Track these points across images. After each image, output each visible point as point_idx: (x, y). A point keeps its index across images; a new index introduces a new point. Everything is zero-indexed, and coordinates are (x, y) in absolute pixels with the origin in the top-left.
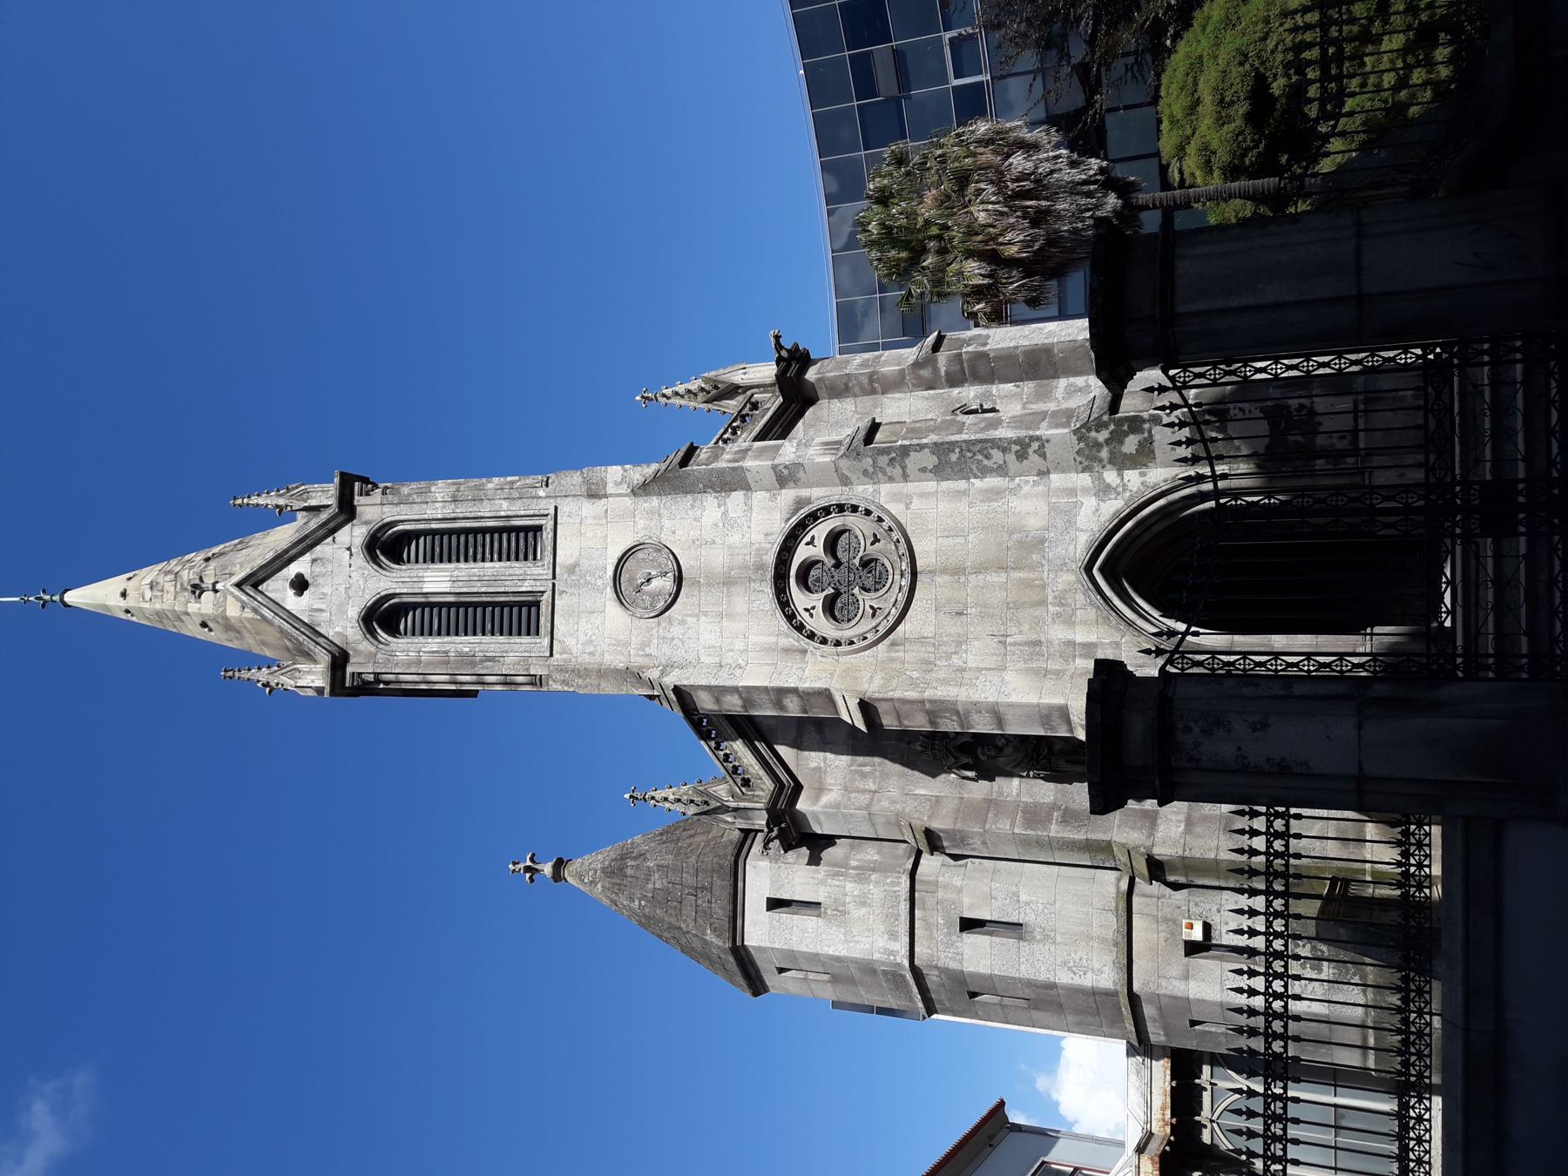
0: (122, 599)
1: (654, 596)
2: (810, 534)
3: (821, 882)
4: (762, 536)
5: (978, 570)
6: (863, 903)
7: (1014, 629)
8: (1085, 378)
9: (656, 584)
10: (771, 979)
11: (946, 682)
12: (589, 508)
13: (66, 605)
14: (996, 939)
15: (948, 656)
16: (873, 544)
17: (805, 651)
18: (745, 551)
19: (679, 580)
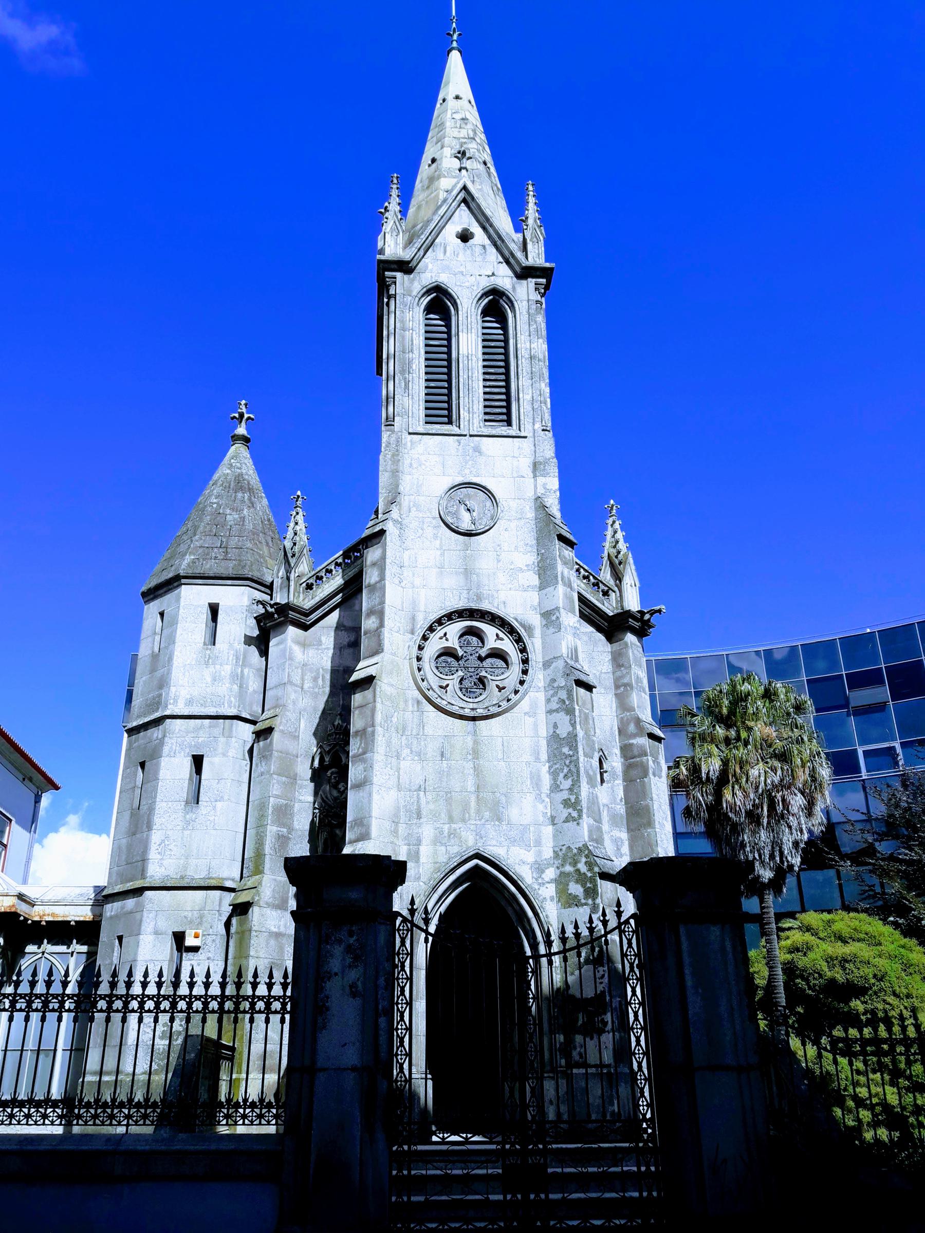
5: (477, 770)
7: (430, 797)
8: (628, 853)
11: (389, 744)
16: (497, 686)
19: (469, 534)
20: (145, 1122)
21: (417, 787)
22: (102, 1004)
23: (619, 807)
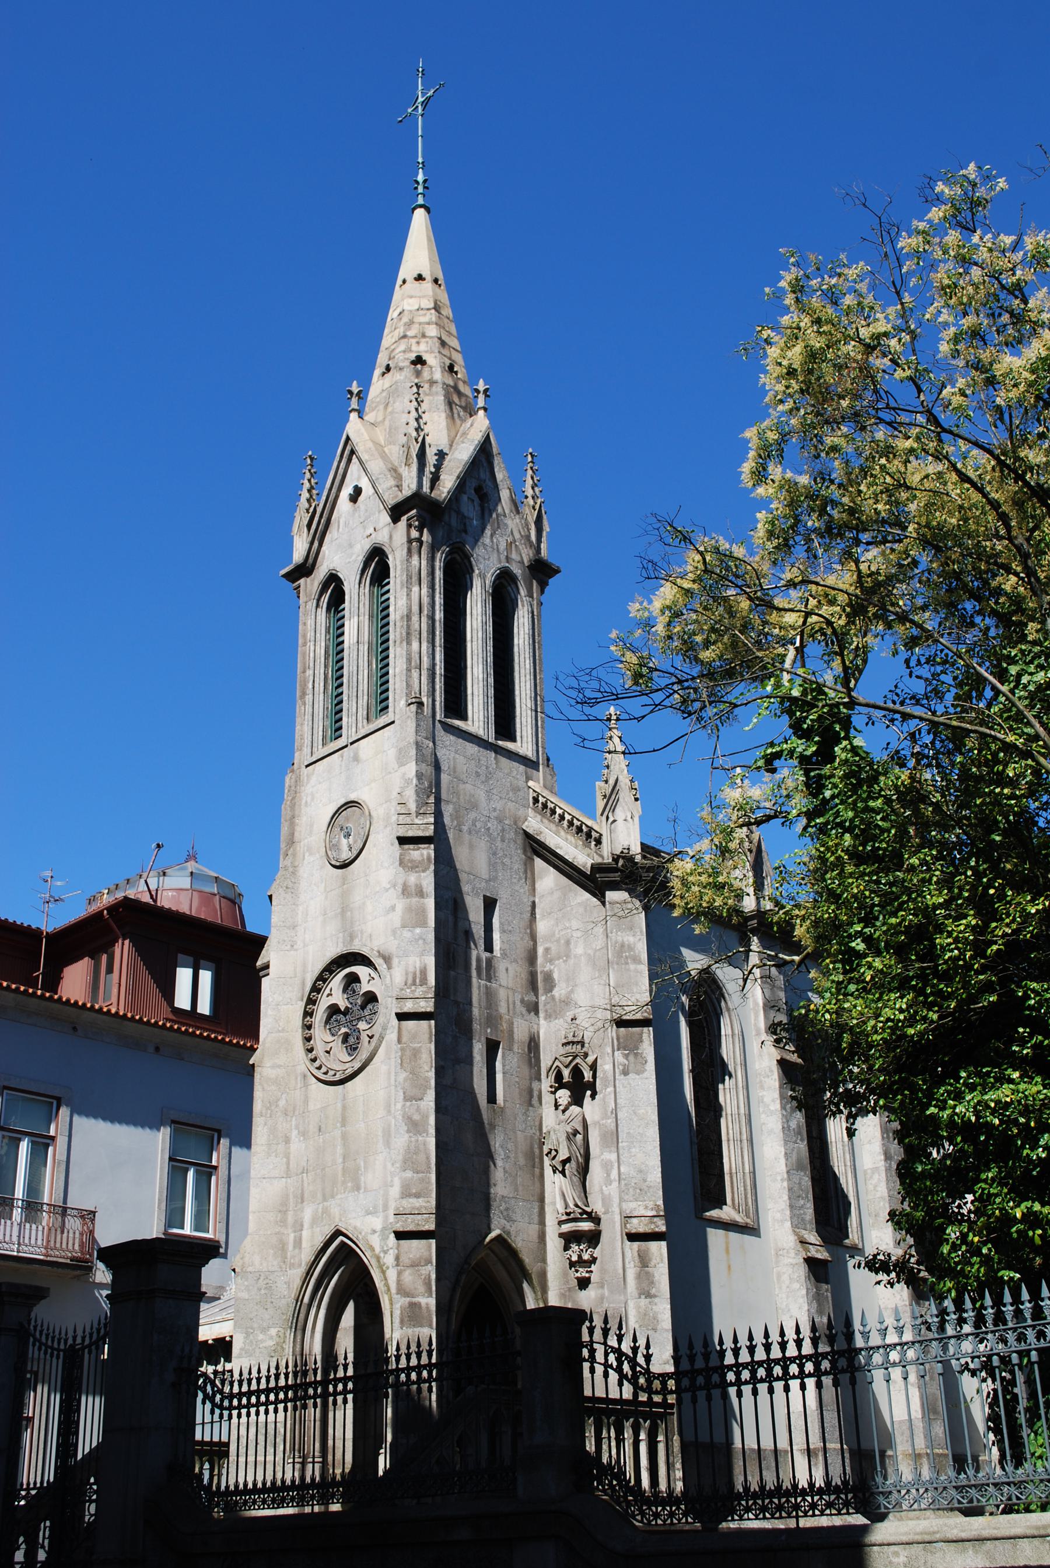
0: (416, 276)
1: (336, 847)
5: (344, 1137)
13: (414, 209)
20: (848, 1510)
21: (300, 1171)
22: (731, 1376)
23: (609, 1121)
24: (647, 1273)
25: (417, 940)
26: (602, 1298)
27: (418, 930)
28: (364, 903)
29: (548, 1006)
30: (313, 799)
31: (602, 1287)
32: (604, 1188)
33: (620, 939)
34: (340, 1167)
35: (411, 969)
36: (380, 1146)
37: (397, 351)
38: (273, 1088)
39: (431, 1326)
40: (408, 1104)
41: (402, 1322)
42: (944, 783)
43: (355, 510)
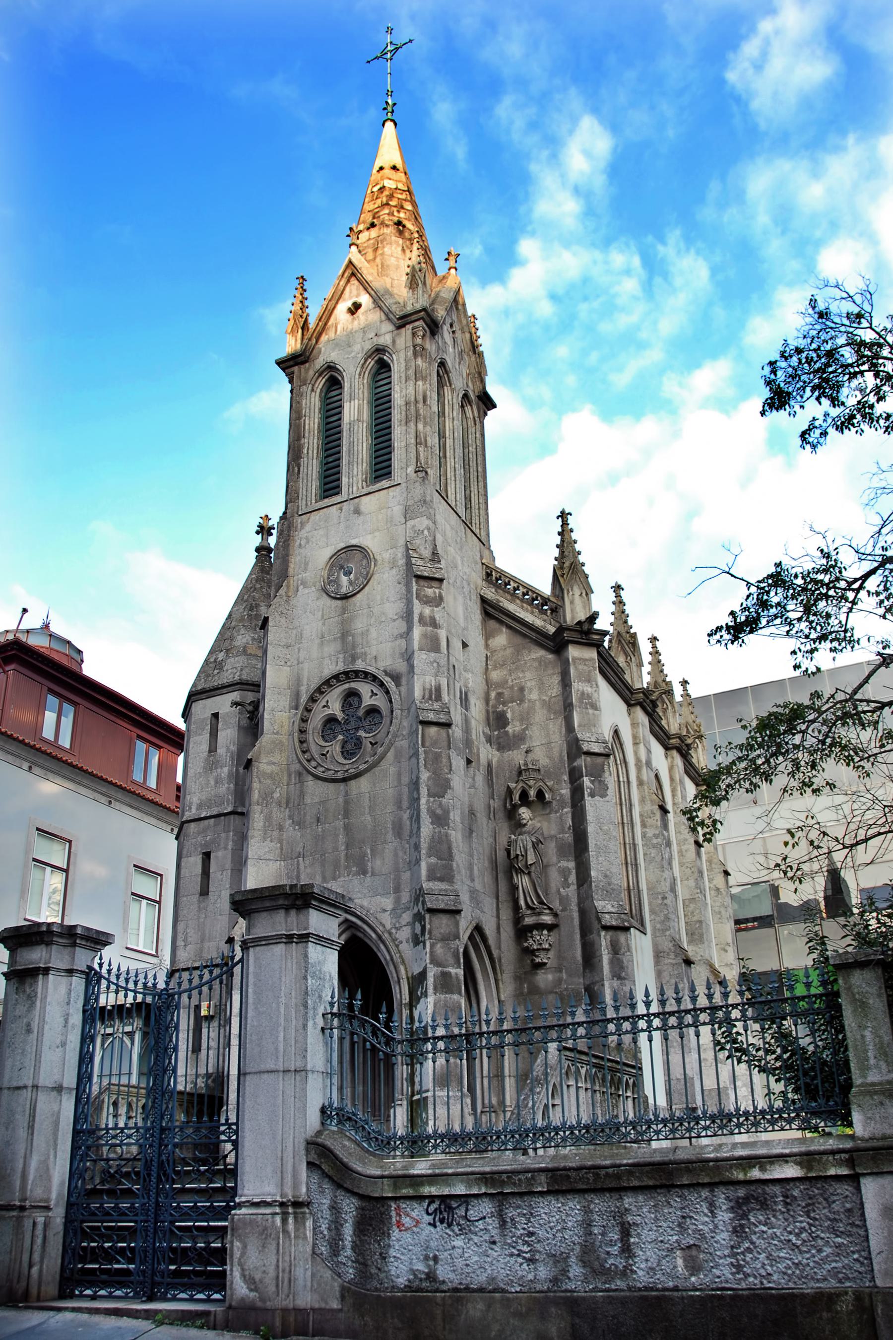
1: (337, 582)
2: (325, 700)
3: (228, 749)
4: (375, 654)
5: (347, 828)
6: (218, 781)
7: (307, 862)
8: (575, 882)
9: (344, 580)
10: (833, 654)
11: (268, 818)
12: (397, 511)
14: (199, 879)
15: (291, 817)
16: (371, 743)
17: (297, 708)
18: (365, 643)
19: (345, 597)
23: (567, 835)
24: (618, 959)
25: (432, 663)
26: (560, 981)
27: (433, 654)
28: (368, 631)
29: (501, 740)
30: (308, 542)
31: (561, 971)
32: (561, 890)
33: (580, 688)
34: (343, 854)
35: (428, 686)
36: (390, 836)
37: (382, 213)
38: (269, 781)
39: (460, 993)
40: (432, 799)
41: (435, 989)
42: (361, 733)
43: (354, 319)
